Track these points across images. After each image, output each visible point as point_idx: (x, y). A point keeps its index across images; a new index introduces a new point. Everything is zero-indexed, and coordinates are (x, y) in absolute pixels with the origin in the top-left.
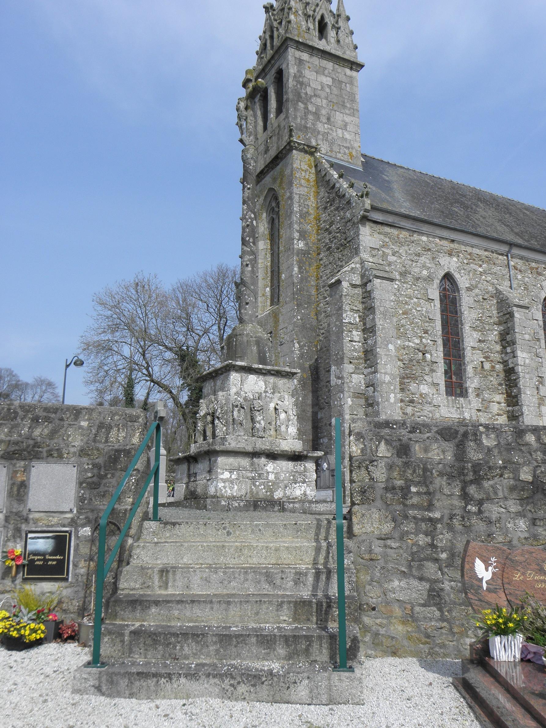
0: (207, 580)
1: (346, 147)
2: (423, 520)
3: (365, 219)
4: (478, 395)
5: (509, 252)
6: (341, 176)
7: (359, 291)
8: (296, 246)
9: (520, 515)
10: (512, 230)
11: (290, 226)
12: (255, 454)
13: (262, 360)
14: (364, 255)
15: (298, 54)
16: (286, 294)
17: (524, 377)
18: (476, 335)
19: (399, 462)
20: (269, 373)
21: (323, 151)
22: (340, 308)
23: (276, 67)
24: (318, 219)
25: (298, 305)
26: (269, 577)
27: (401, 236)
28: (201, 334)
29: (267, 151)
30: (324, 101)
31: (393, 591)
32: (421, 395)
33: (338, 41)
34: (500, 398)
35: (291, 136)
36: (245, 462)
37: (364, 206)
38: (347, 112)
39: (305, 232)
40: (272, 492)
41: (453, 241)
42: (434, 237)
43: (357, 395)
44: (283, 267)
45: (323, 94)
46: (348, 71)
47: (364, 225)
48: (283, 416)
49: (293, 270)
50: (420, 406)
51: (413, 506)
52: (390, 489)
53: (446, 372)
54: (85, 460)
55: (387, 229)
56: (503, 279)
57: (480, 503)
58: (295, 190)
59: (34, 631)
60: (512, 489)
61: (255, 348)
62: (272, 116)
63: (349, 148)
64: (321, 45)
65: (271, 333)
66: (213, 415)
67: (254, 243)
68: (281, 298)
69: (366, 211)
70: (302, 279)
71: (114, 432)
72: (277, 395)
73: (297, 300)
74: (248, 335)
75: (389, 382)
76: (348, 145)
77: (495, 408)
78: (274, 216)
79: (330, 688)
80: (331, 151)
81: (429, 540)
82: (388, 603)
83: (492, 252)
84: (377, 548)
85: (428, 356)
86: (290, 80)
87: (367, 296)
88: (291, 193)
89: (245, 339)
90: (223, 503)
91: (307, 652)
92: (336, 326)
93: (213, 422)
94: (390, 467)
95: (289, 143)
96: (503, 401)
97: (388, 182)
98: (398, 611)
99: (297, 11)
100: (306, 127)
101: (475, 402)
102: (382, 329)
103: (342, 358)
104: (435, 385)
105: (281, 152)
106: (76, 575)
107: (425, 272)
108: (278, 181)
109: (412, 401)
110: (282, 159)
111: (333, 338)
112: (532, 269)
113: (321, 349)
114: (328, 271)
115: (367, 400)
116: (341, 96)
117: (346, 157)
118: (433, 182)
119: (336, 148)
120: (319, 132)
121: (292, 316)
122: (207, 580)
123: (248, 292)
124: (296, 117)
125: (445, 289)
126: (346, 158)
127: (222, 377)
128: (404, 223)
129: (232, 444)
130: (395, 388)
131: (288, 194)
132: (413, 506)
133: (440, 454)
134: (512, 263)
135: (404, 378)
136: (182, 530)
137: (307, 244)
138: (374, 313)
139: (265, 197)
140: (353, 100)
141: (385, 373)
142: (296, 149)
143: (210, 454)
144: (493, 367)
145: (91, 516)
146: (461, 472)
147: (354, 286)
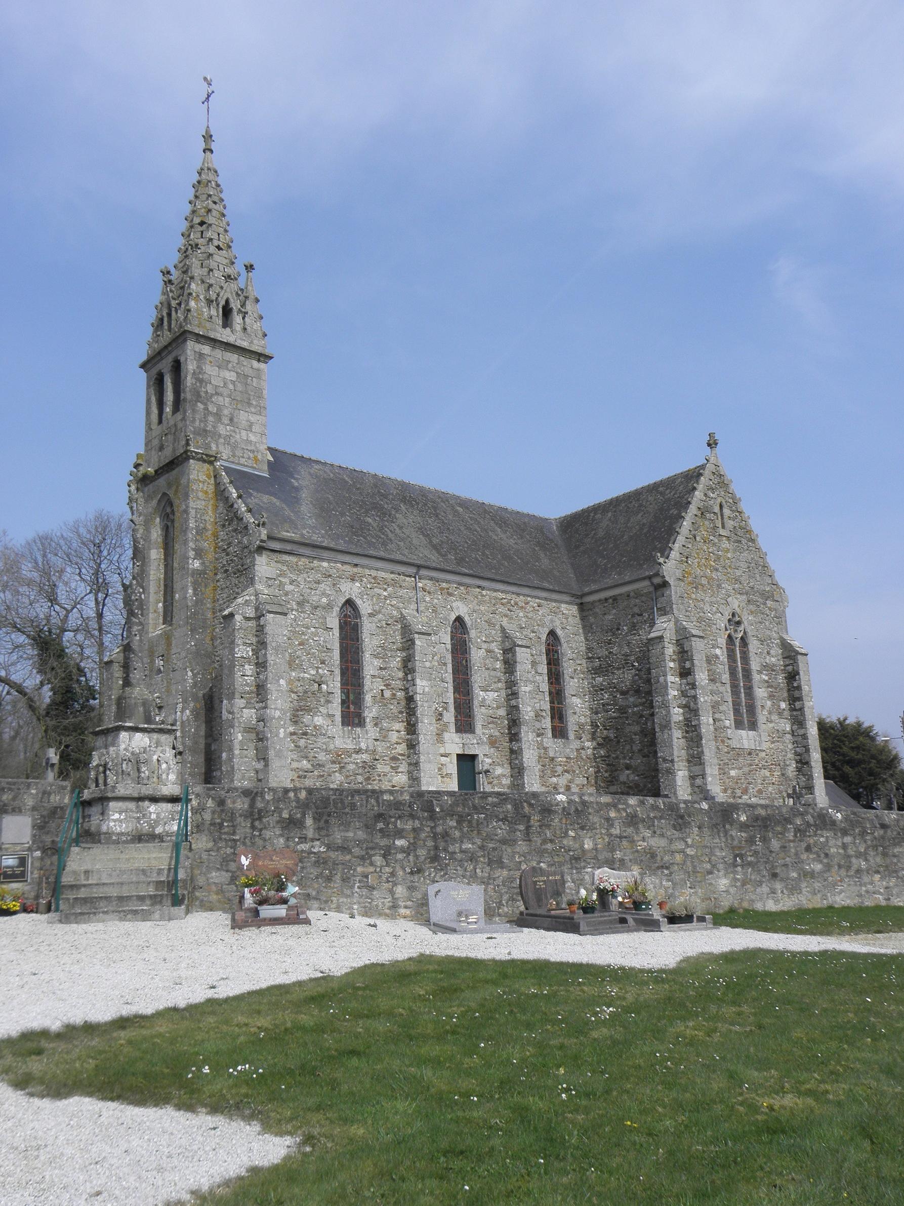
0: (110, 875)
1: (250, 451)
2: (230, 840)
3: (261, 549)
4: (376, 725)
5: (417, 573)
6: (240, 497)
7: (252, 624)
8: (191, 566)
9: (281, 835)
10: (431, 542)
11: (185, 542)
12: (140, 799)
13: (148, 720)
14: (260, 587)
15: (198, 347)
16: (179, 617)
17: (422, 706)
18: (377, 663)
19: (218, 809)
20: (153, 731)
21: (225, 457)
22: (233, 642)
23: (173, 355)
24: (216, 536)
25: (191, 630)
26: (144, 872)
27: (300, 563)
28: (69, 607)
29: (161, 448)
30: (227, 400)
31: (212, 878)
32: (315, 727)
33: (245, 329)
34: (400, 726)
35: (188, 444)
36: (132, 805)
37: (260, 536)
38: (253, 410)
39: (202, 550)
40: (154, 828)
41: (356, 565)
42: (336, 562)
43: (248, 730)
44: (177, 586)
45: (226, 392)
46: (255, 364)
47: (260, 554)
48: (164, 766)
49: (187, 592)
50: (313, 738)
51: (225, 833)
52: (213, 824)
53: (343, 702)
54: (35, 813)
55: (286, 558)
56: (409, 602)
57: (261, 830)
58: (192, 504)
59: (14, 906)
60: (278, 822)
61: (141, 709)
62: (168, 410)
63: (253, 452)
64: (225, 335)
65: (163, 656)
66: (105, 766)
67: (142, 615)
68: (174, 620)
69: (262, 541)
70: (197, 602)
71: (52, 797)
72: (160, 748)
73: (191, 624)
74: (135, 698)
75: (279, 717)
76: (253, 448)
77: (394, 737)
78: (169, 524)
79: (169, 914)
80: (234, 456)
81: (232, 850)
82: (209, 885)
83: (399, 574)
84: (205, 856)
85: (324, 687)
86: (189, 378)
87: (260, 630)
88: (187, 507)
89: (133, 701)
90: (114, 838)
91: (161, 902)
92: (229, 659)
93: (104, 772)
94: (213, 812)
95: (186, 452)
96: (403, 729)
97: (297, 489)
98: (214, 888)
99: (198, 296)
100: (205, 431)
101: (372, 731)
102: (274, 664)
103: (233, 693)
104: (331, 716)
105: (177, 458)
106: (32, 878)
107: (324, 600)
108: (174, 488)
109: (305, 734)
110: (178, 465)
111: (226, 671)
112: (442, 589)
113: (216, 677)
114: (225, 595)
115: (257, 734)
116: (246, 393)
117: (250, 461)
118: (352, 479)
119: (239, 453)
120: (220, 435)
121: (185, 642)
122: (110, 875)
123: (136, 658)
124: (194, 420)
125: (345, 616)
126: (250, 463)
127: (113, 734)
128: (302, 550)
129: (121, 791)
130: (285, 724)
131: (184, 507)
132: (225, 833)
133: (241, 804)
134: (420, 585)
135: (298, 710)
136: (91, 851)
137: (203, 564)
138: (266, 648)
139: (159, 501)
140: (260, 397)
141: (276, 709)
142: (193, 458)
143: (103, 800)
144: (394, 695)
145: (40, 845)
146: (252, 814)
147: (248, 619)
